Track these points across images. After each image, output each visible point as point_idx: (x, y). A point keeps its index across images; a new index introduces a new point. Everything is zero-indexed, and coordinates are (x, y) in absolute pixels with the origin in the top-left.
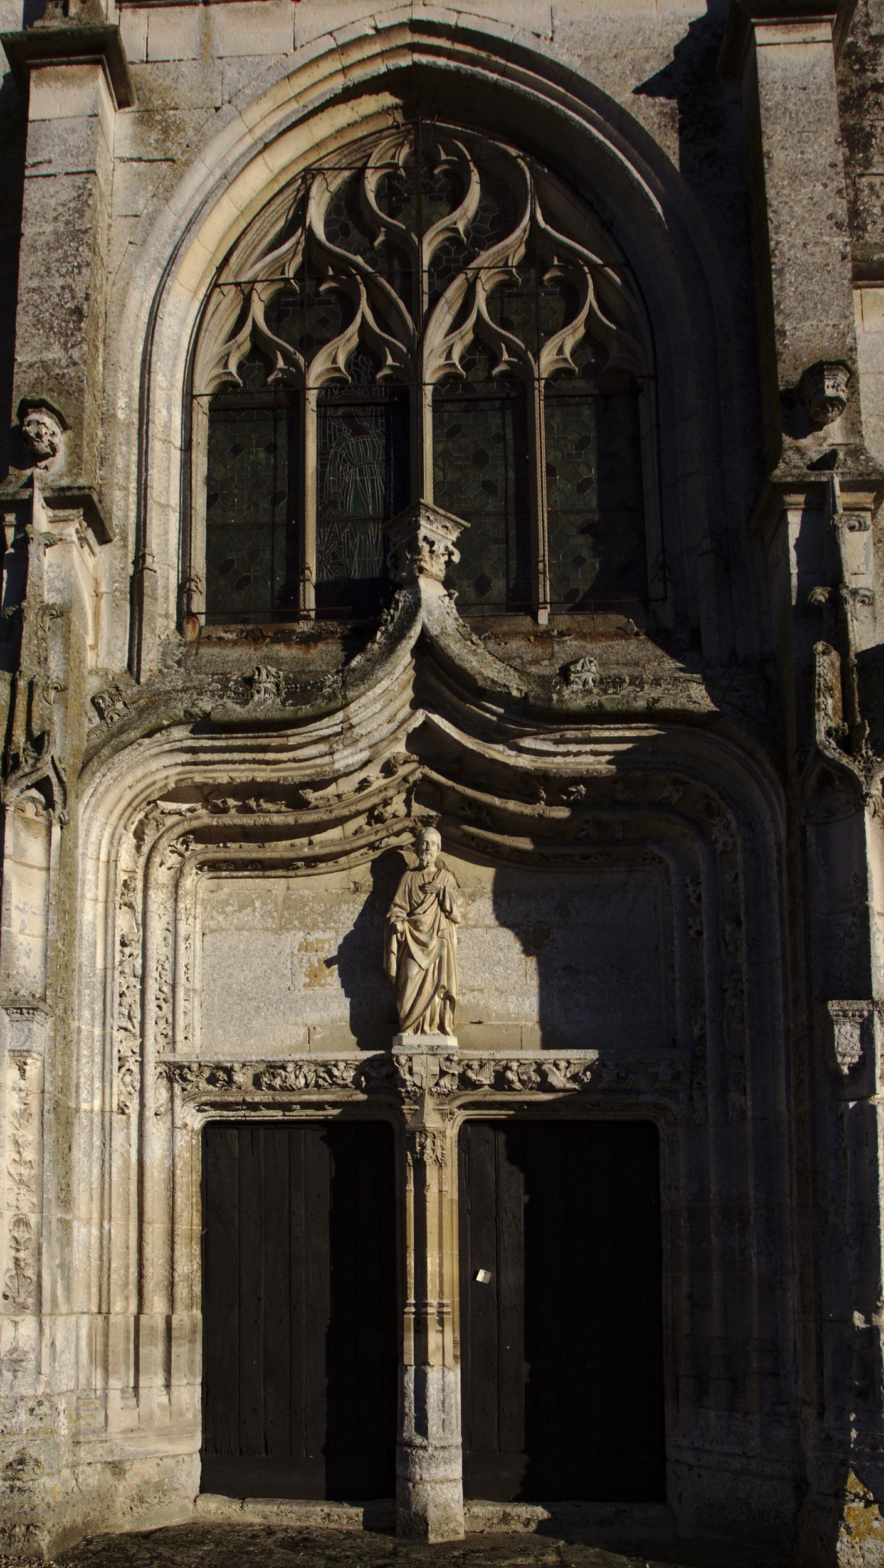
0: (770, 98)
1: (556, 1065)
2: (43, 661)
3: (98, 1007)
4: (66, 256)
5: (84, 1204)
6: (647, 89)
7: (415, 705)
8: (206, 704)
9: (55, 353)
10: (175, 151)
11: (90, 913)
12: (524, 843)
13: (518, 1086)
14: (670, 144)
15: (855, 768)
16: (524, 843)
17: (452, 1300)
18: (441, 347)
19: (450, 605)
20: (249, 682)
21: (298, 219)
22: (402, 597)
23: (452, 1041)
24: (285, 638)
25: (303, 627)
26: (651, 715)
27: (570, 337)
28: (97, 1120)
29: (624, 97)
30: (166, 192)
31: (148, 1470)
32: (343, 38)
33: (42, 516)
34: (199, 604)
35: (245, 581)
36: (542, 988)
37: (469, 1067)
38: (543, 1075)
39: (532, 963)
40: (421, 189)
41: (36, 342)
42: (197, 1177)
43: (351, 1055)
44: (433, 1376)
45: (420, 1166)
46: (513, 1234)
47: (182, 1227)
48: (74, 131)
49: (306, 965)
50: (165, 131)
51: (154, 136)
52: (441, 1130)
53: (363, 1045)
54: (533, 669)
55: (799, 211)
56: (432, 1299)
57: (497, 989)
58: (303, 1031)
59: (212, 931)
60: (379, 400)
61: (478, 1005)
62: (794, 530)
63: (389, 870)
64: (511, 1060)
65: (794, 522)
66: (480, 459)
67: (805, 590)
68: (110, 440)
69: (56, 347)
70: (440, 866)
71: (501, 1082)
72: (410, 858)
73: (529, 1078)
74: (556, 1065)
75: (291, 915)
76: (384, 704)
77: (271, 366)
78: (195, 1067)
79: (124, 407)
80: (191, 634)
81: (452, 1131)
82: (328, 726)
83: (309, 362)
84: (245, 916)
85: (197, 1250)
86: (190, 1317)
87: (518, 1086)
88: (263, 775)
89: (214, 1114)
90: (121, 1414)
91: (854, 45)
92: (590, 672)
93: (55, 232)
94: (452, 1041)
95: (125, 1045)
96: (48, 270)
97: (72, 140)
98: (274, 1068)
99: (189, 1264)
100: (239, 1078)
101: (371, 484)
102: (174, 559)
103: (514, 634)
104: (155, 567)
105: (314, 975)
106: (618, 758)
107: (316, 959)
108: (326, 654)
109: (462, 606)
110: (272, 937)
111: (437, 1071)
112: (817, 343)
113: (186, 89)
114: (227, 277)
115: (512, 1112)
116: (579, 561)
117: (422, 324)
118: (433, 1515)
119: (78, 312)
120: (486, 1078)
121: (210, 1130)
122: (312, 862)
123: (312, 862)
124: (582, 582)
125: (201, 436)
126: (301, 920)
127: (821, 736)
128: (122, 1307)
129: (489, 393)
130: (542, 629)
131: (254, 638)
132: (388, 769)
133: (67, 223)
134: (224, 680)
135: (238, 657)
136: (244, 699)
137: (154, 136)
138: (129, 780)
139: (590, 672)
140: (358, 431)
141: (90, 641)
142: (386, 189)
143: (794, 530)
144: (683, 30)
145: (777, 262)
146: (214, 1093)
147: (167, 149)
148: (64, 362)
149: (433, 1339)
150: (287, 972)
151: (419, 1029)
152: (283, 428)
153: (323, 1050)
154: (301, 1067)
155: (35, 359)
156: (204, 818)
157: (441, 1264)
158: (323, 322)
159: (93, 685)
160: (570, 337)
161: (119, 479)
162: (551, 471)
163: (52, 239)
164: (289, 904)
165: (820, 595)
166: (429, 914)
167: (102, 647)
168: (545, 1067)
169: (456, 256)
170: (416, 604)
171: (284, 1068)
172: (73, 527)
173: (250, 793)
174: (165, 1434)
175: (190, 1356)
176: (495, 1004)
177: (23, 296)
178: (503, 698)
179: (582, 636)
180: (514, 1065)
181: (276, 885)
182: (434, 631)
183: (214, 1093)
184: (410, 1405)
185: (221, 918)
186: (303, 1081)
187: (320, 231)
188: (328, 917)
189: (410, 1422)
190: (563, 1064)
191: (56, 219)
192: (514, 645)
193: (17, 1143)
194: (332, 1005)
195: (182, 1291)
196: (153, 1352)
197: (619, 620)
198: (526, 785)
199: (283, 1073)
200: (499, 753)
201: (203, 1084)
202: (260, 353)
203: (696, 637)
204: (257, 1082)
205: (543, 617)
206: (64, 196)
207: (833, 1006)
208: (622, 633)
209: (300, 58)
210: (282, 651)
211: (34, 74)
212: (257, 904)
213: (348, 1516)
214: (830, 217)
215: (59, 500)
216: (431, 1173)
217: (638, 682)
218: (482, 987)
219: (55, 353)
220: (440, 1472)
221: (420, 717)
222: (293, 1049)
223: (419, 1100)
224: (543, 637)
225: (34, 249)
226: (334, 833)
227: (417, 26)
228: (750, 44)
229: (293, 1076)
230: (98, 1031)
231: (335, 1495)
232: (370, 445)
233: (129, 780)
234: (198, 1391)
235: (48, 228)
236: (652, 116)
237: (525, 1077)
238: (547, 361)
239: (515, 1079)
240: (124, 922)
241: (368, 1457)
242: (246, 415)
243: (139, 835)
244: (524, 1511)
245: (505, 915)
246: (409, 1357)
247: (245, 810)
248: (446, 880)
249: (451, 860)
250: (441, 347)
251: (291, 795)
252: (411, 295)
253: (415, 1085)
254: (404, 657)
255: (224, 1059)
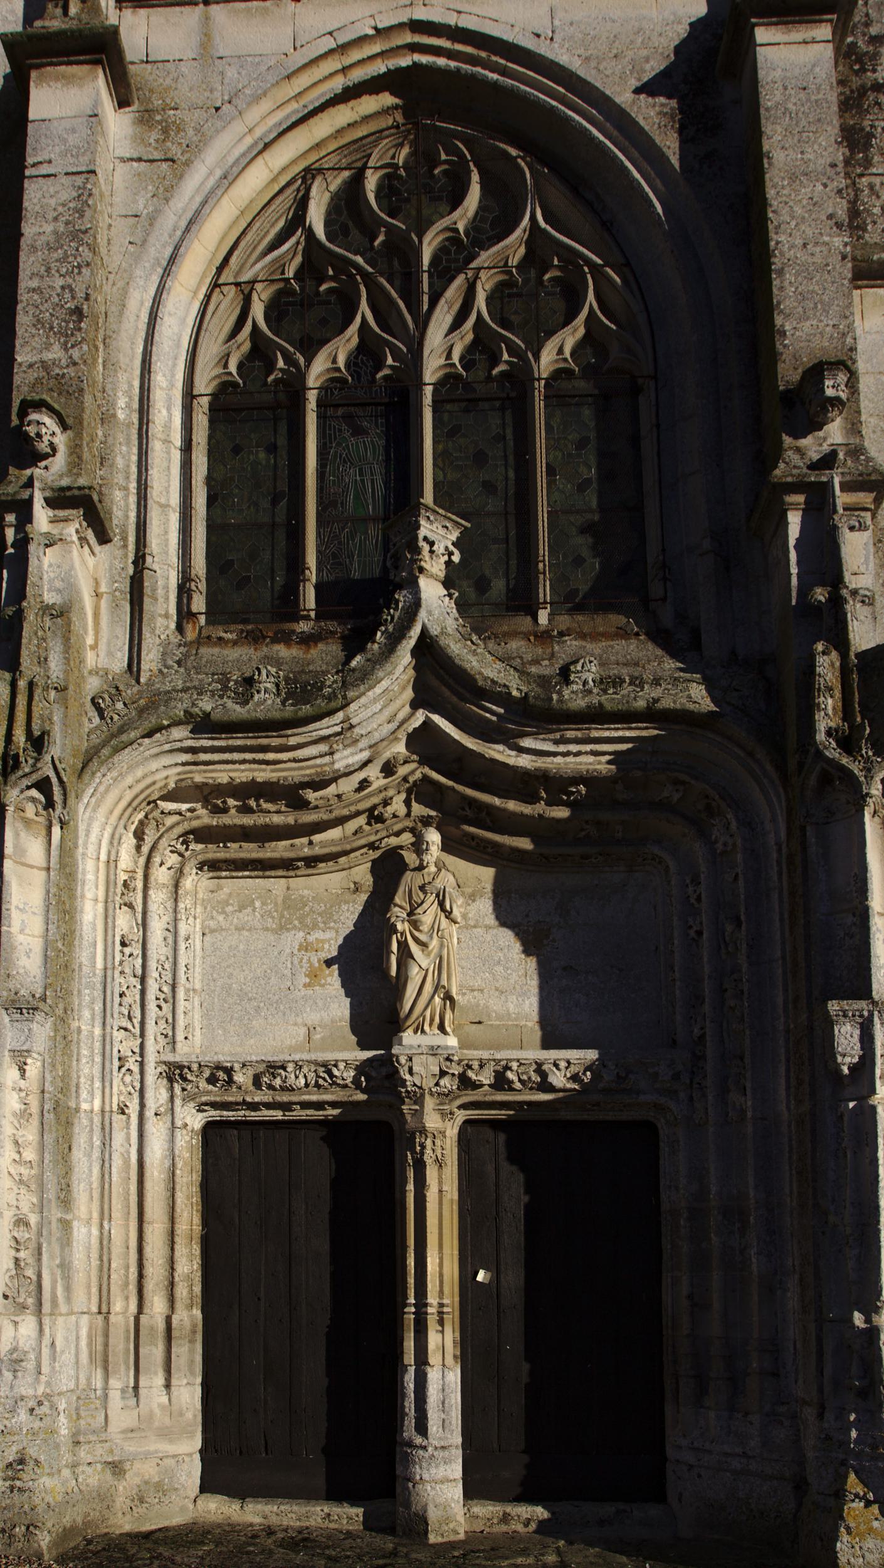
0: (770, 98)
1: (556, 1065)
2: (43, 661)
3: (98, 1007)
4: (66, 256)
5: (84, 1204)
6: (647, 89)
7: (415, 705)
8: (206, 704)
9: (55, 353)
10: (175, 151)
11: (90, 913)
12: (524, 843)
13: (518, 1086)
14: (670, 144)
15: (855, 768)
16: (524, 843)
17: (452, 1300)
18: (441, 347)
19: (450, 605)
20: (249, 682)
21: (298, 219)
22: (402, 597)
23: (452, 1041)
24: (285, 638)
25: (303, 627)
26: (651, 715)
27: (570, 337)
28: (97, 1120)
29: (624, 97)
30: (166, 192)
31: (148, 1470)
32: (343, 38)
33: (42, 516)
34: (199, 604)
35: (245, 581)
36: (542, 988)
37: (469, 1067)
38: (543, 1075)
39: (532, 963)
40: (421, 189)
41: (36, 342)
42: (197, 1177)
43: (351, 1055)
44: (433, 1376)
45: (420, 1166)
46: (513, 1234)
47: (182, 1227)
48: (74, 131)
49: (306, 965)
50: (165, 131)
51: (154, 136)
52: (441, 1130)
53: (363, 1045)
54: (533, 669)
55: (799, 211)
56: (432, 1299)
57: (497, 989)
58: (303, 1031)
59: (212, 931)
60: (379, 400)
61: (478, 1005)
62: (794, 530)
63: (389, 870)
64: (511, 1060)
65: (794, 522)
66: (480, 459)
67: (805, 590)
68: (110, 440)
69: (56, 347)
70: (440, 866)
71: (501, 1082)
72: (410, 858)
73: (529, 1078)
74: (556, 1065)
75: (291, 915)
76: (384, 704)
77: (271, 366)
78: (195, 1067)
79: (124, 407)
80: (191, 634)
81: (452, 1131)
82: (328, 726)
83: (309, 362)
84: (245, 916)
85: (197, 1250)
86: (190, 1317)
87: (518, 1086)
88: (263, 775)
89: (214, 1114)
90: (121, 1414)
91: (854, 45)
92: (590, 672)
93: (55, 232)
94: (452, 1041)
95: (125, 1045)
96: (48, 270)
97: (72, 140)
98: (274, 1068)
99: (189, 1264)
100: (239, 1078)
101: (371, 484)
102: (174, 559)
103: (514, 634)
104: (155, 567)
105: (314, 975)
106: (618, 758)
107: (316, 959)
108: (326, 654)
109: (462, 606)
110: (272, 937)
111: (437, 1071)
112: (817, 343)
113: (186, 89)
114: (227, 277)
115: (512, 1112)
116: (579, 561)
117: (422, 324)
118: (433, 1515)
119: (78, 312)
120: (486, 1078)
121: (210, 1130)
122: (312, 862)
123: (312, 862)
124: (582, 582)
125: (201, 436)
126: (301, 920)
127: (821, 736)
128: (122, 1307)
129: (489, 393)
130: (542, 629)
131: (254, 638)
132: (388, 769)
133: (67, 223)
134: (224, 680)
135: (238, 657)
136: (244, 699)
137: (154, 136)
138: (129, 780)
139: (590, 672)
140: (358, 431)
141: (90, 641)
142: (386, 189)
143: (794, 530)
144: (683, 30)
145: (777, 262)
146: (214, 1093)
147: (167, 149)
148: (64, 362)
149: (433, 1339)
150: (287, 972)
151: (419, 1029)
152: (283, 428)
153: (323, 1050)
154: (301, 1067)
155: (35, 359)
156: (204, 818)
157: (441, 1264)
158: (323, 322)
159: (93, 685)
160: (570, 337)
161: (119, 479)
162: (551, 471)
163: (52, 239)
164: (289, 904)
165: (820, 595)
166: (429, 914)
167: (102, 647)
168: (545, 1067)
169: (456, 256)
170: (416, 604)
171: (284, 1068)
172: (73, 527)
173: (250, 793)
174: (165, 1434)
175: (190, 1356)
176: (495, 1004)
177: (23, 296)
178: (503, 698)
179: (582, 636)
180: (514, 1065)
181: (276, 885)
182: (434, 631)
183: (214, 1093)
184: (410, 1405)
185: (221, 918)
186: (303, 1081)
187: (320, 231)
188: (328, 917)
189: (410, 1422)
190: (563, 1064)
191: (56, 219)
192: (514, 645)
193: (17, 1143)
194: (332, 1005)
195: (182, 1291)
196: (153, 1352)
197: (619, 620)
198: (526, 785)
199: (283, 1073)
200: (499, 753)
201: (203, 1084)
202: (260, 353)
203: (696, 637)
204: (257, 1082)
205: (543, 617)
206: (64, 196)
207: (833, 1006)
208: (622, 633)
209: (300, 58)
210: (282, 651)
211: (34, 74)
212: (257, 904)
213: (348, 1516)
214: (830, 217)
215: (59, 500)
216: (431, 1173)
217: (638, 682)
218: (482, 987)
219: (55, 353)
220: (440, 1472)
221: (420, 717)
222: (293, 1049)
223: (419, 1100)
224: (543, 637)
225: (34, 249)
226: (334, 833)
227: (417, 26)
228: (750, 44)
229: (293, 1076)
230: (98, 1031)
231: (335, 1495)
232: (370, 445)
233: (129, 780)
234: (198, 1391)
235: (48, 228)
236: (652, 116)
237: (525, 1077)
238: (547, 361)
239: (515, 1079)
240: (124, 922)
241: (368, 1457)
242: (246, 415)
243: (139, 835)
244: (524, 1511)
245: (505, 915)
246: (409, 1357)
247: (245, 810)
248: (446, 880)
249: (451, 860)
250: (441, 347)
251: (291, 795)
252: (411, 295)
253: (415, 1085)
254: (404, 657)
255: (224, 1059)
